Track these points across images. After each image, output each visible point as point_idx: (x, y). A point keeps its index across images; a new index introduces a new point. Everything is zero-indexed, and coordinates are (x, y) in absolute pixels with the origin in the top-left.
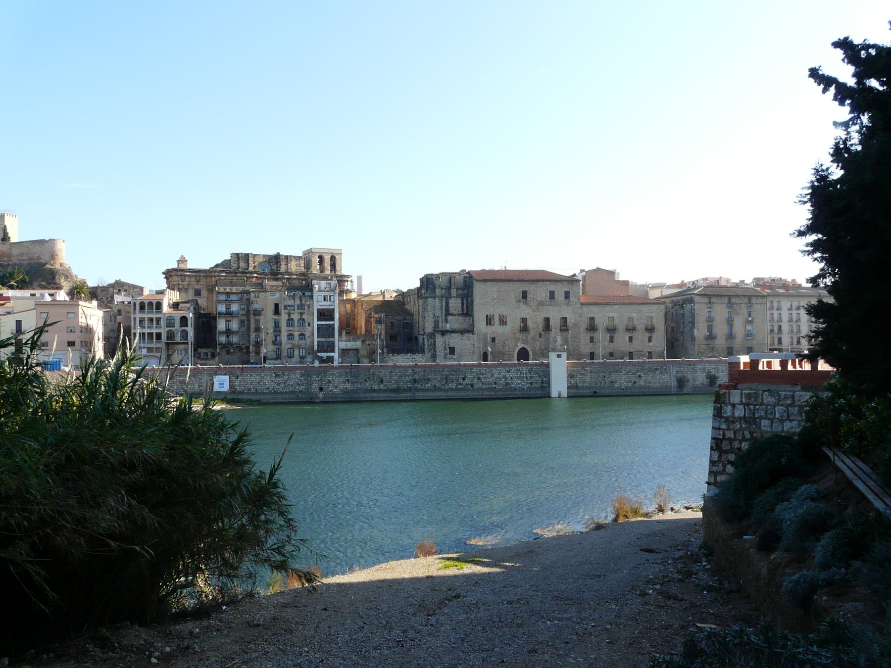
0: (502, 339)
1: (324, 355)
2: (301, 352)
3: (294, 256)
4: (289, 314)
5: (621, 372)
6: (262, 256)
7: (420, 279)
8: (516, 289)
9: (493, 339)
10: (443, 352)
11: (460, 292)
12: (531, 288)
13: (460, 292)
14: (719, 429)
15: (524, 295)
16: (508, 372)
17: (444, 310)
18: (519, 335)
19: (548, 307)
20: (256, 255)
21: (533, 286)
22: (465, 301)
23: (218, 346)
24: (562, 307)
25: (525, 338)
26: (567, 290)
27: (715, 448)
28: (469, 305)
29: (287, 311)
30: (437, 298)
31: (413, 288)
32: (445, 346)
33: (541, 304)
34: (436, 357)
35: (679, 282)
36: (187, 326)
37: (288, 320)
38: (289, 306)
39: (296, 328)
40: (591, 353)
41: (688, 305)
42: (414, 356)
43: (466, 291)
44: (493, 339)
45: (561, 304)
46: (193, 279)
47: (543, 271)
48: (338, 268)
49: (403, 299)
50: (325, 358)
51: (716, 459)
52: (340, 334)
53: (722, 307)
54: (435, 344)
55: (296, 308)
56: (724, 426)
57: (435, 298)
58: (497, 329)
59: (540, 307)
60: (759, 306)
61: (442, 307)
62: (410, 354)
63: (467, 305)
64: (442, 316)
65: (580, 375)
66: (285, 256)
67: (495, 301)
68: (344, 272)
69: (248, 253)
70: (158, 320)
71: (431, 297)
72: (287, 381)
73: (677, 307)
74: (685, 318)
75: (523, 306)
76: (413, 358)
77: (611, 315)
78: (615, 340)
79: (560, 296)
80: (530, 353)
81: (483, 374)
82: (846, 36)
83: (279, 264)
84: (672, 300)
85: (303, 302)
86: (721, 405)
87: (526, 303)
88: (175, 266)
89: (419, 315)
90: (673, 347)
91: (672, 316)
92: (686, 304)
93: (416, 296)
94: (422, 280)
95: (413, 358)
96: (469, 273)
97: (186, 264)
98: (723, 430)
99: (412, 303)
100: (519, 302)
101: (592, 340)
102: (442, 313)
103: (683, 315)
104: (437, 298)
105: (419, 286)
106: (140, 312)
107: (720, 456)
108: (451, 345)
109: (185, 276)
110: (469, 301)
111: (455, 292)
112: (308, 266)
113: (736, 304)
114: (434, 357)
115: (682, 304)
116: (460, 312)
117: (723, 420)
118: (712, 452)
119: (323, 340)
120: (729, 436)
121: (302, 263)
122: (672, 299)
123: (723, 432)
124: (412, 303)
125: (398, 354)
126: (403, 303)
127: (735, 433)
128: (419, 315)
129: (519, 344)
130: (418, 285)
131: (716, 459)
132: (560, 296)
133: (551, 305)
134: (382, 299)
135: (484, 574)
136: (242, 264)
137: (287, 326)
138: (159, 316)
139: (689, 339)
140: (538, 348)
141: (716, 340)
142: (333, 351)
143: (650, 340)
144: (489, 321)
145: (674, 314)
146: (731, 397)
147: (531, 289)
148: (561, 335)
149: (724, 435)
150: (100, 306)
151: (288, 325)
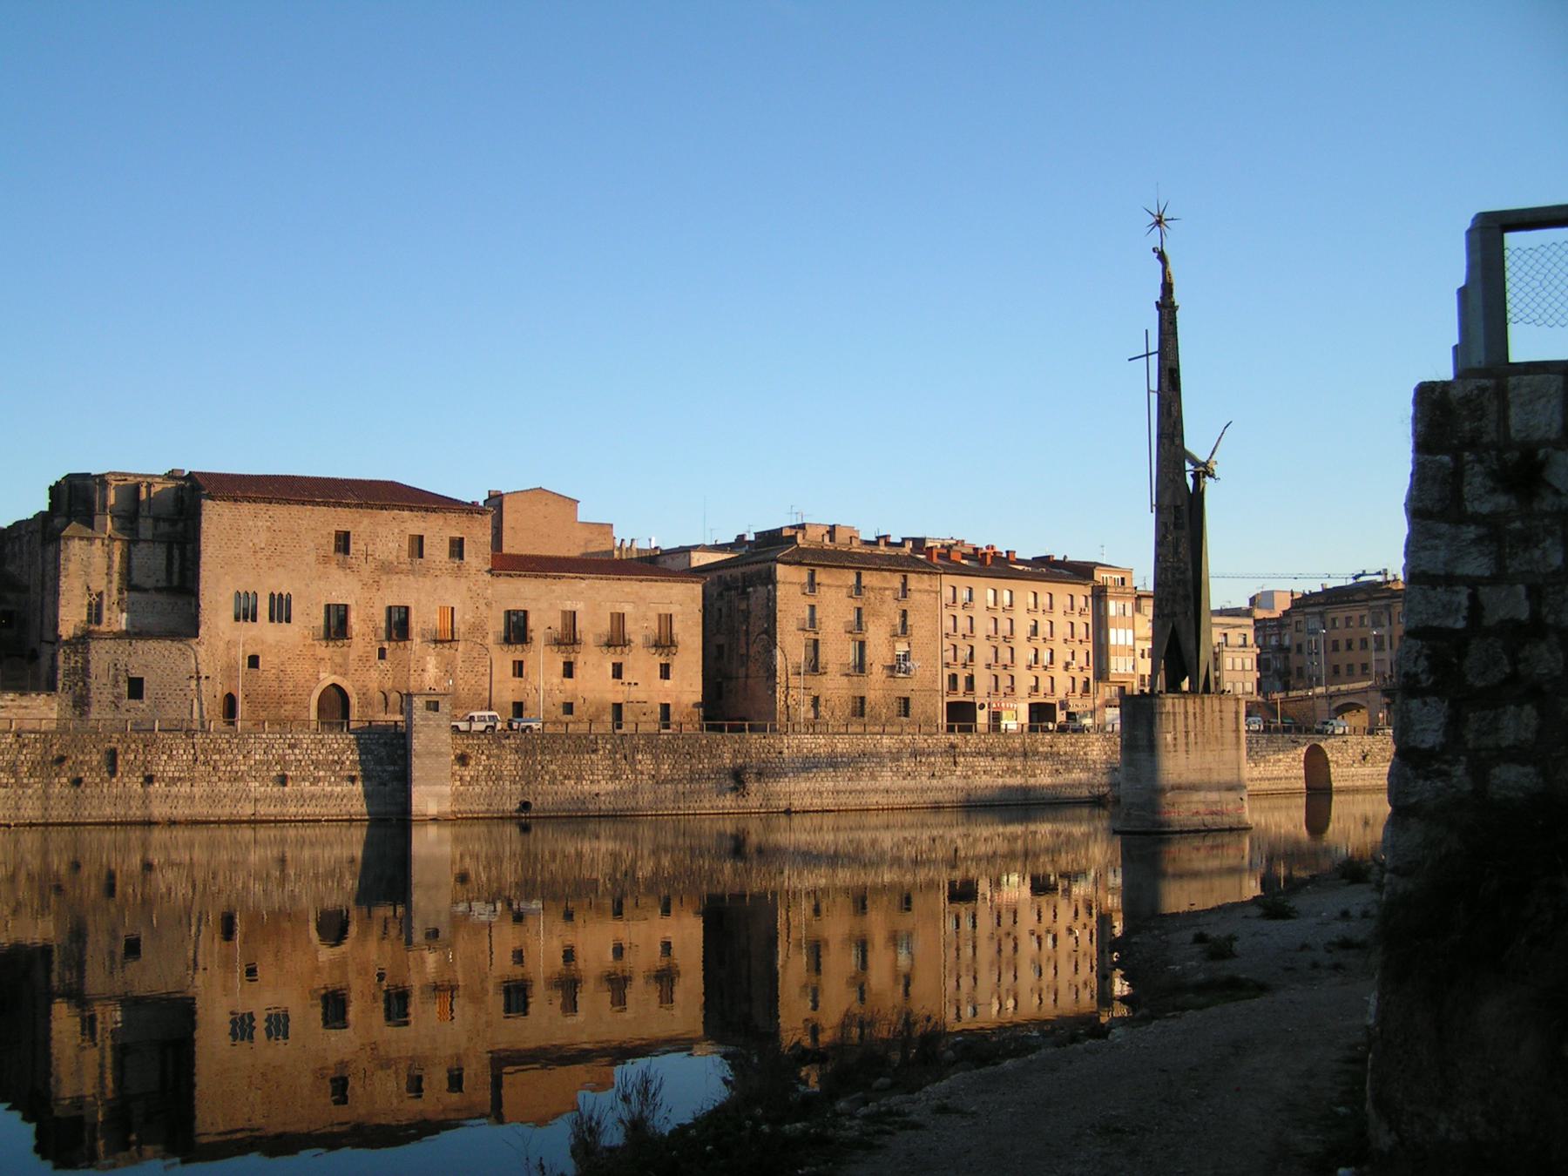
0: (277, 661)
5: (595, 751)
7: (51, 488)
9: (254, 661)
10: (109, 689)
11: (164, 527)
12: (360, 523)
13: (164, 527)
14: (1450, 580)
15: (343, 542)
17: (116, 577)
18: (323, 650)
19: (402, 576)
21: (366, 521)
22: (176, 553)
24: (442, 579)
25: (338, 660)
26: (458, 535)
27: (1426, 681)
33: (386, 568)
34: (88, 705)
35: (732, 540)
41: (759, 588)
42: (25, 701)
43: (181, 525)
44: (254, 661)
45: (438, 573)
51: (1430, 736)
54: (85, 671)
56: (1476, 565)
57: (91, 540)
58: (265, 632)
59: (384, 578)
60: (925, 597)
61: (110, 567)
62: (11, 696)
64: (109, 590)
65: (488, 759)
67: (260, 555)
71: (81, 539)
74: (752, 621)
75: (335, 572)
76: (20, 707)
77: (569, 606)
78: (577, 672)
79: (437, 551)
82: (741, 533)
84: (720, 577)
86: (1457, 458)
87: (344, 566)
89: (43, 589)
90: (720, 696)
91: (721, 617)
93: (38, 536)
94: (55, 491)
95: (20, 707)
96: (191, 476)
98: (1473, 583)
101: (519, 670)
102: (110, 582)
105: (46, 508)
107: (1454, 724)
108: (135, 674)
111: (141, 530)
113: (872, 589)
114: (81, 703)
116: (162, 584)
117: (1471, 532)
118: (1415, 703)
120: (1502, 614)
123: (1473, 598)
127: (1535, 593)
129: (322, 676)
130: (43, 504)
131: (1430, 736)
133: (412, 572)
135: (726, 560)
139: (761, 672)
143: (665, 672)
144: (246, 613)
146: (1513, 411)
147: (361, 528)
148: (438, 655)
149: (1476, 608)
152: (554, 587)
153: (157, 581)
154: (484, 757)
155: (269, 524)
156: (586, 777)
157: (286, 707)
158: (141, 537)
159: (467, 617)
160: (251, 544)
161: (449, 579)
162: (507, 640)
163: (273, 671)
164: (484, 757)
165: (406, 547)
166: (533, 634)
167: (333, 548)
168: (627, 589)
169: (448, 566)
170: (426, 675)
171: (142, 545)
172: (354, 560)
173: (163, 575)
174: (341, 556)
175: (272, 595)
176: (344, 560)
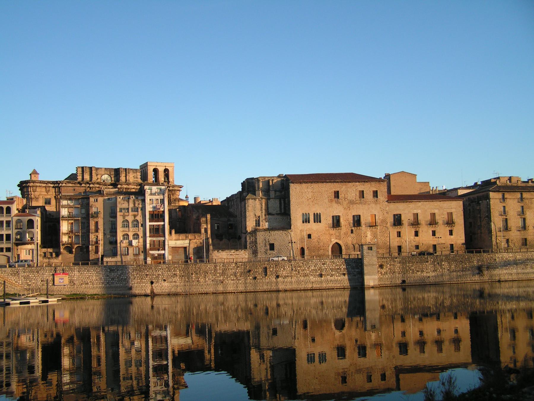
1: (156, 253)
2: (135, 250)
3: (131, 169)
4: (124, 216)
6: (103, 169)
7: (242, 183)
8: (330, 188)
9: (309, 236)
11: (278, 194)
12: (342, 188)
13: (278, 194)
15: (337, 194)
16: (323, 264)
20: (98, 168)
21: (344, 187)
22: (282, 202)
23: (61, 247)
25: (337, 234)
26: (375, 189)
28: (286, 205)
29: (122, 214)
30: (257, 200)
31: (236, 193)
32: (265, 243)
33: (352, 202)
34: (257, 253)
36: (33, 228)
37: (123, 221)
38: (124, 209)
39: (131, 229)
40: (398, 246)
41: (484, 201)
42: (237, 253)
43: (283, 193)
44: (309, 236)
45: (369, 203)
46: (44, 189)
47: (352, 173)
48: (171, 180)
49: (228, 204)
50: (156, 255)
52: (170, 233)
53: (515, 202)
54: (256, 242)
55: (130, 210)
58: (312, 226)
59: (351, 206)
61: (261, 208)
62: (233, 251)
63: (284, 205)
64: (262, 215)
65: (390, 266)
66: (123, 169)
67: (310, 201)
68: (176, 183)
69: (91, 166)
70: (8, 223)
71: (252, 199)
72: (120, 275)
73: (474, 203)
74: (482, 213)
75: (335, 205)
76: (236, 254)
77: (415, 212)
78: (420, 234)
79: (369, 195)
80: (333, 325)
81: (300, 267)
83: (118, 176)
85: (136, 205)
87: (337, 203)
88: (28, 178)
92: (482, 200)
93: (239, 199)
94: (243, 184)
95: (236, 254)
97: (38, 177)
99: (235, 206)
100: (331, 201)
101: (399, 234)
103: (480, 211)
104: (257, 200)
106: (6, 229)
108: (271, 242)
109: (36, 187)
110: (287, 202)
111: (274, 194)
112: (144, 177)
114: (255, 252)
115: (478, 202)
116: (279, 212)
119: (154, 239)
121: (139, 174)
122: (468, 197)
124: (235, 206)
125: (223, 251)
126: (228, 207)
128: (241, 216)
129: (332, 240)
130: (240, 189)
132: (369, 195)
133: (361, 203)
134: (211, 204)
136: (87, 177)
137: (122, 227)
138: (9, 219)
140: (350, 243)
141: (510, 232)
142: (164, 249)
143: (451, 233)
144: (306, 220)
145: (471, 210)
147: (342, 189)
148: (371, 231)
150: (248, 389)
151: (123, 226)
152: (410, 205)
153: (277, 211)
154: (389, 265)
155: (312, 190)
156: (425, 271)
157: (321, 251)
158: (271, 197)
159: (380, 217)
160: (306, 197)
161: (373, 205)
162: (395, 225)
163: (316, 239)
164: (389, 265)
165: (358, 194)
166: (403, 222)
167: (333, 197)
168: (436, 205)
169: (373, 200)
170: (367, 238)
171: (271, 200)
172: (341, 201)
173: (278, 209)
174: (336, 199)
175: (314, 214)
176: (338, 201)
